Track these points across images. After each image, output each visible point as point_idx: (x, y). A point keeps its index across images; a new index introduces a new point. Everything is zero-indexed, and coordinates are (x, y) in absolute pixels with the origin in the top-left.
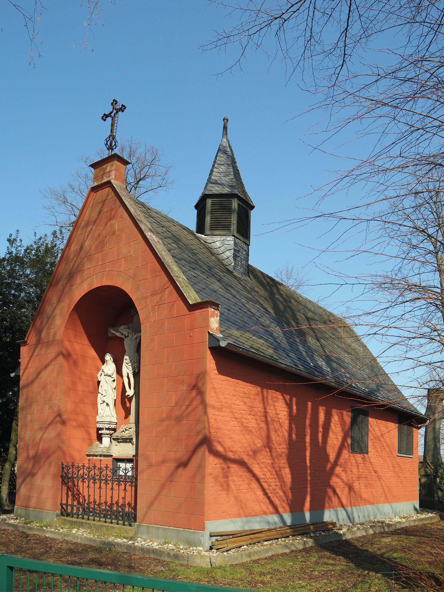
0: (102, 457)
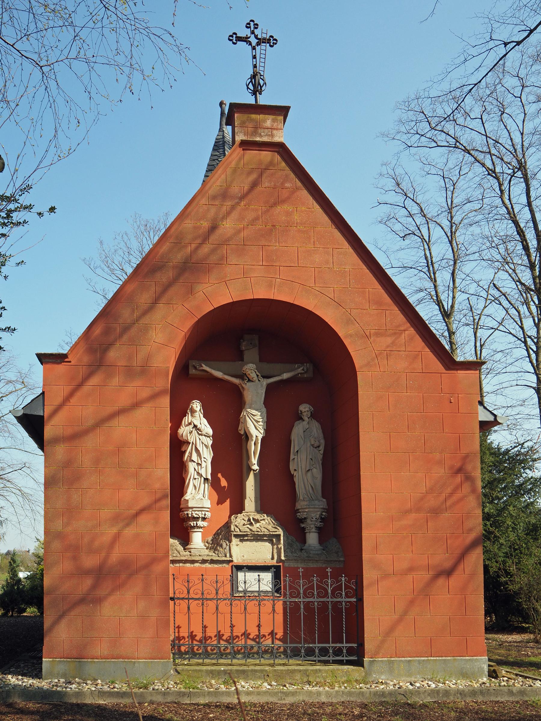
0: (207, 564)
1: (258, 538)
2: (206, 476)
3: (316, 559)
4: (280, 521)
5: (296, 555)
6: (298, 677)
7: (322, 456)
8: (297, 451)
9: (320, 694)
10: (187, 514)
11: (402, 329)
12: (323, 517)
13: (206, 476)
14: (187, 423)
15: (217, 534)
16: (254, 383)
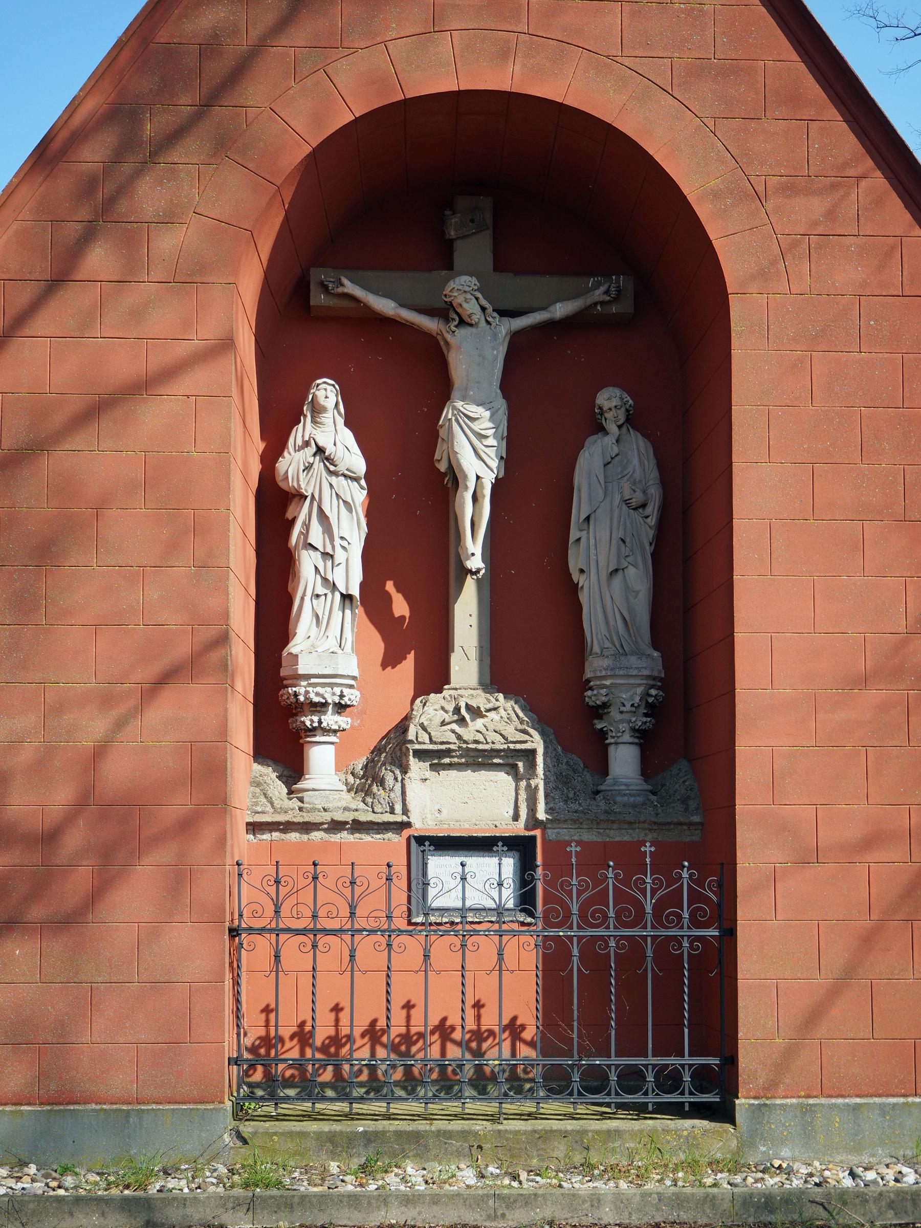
0: (344, 834)
1: (478, 759)
2: (347, 589)
3: (628, 819)
4: (540, 714)
5: (575, 806)
6: (559, 1150)
7: (651, 533)
8: (588, 519)
9: (599, 1200)
10: (296, 695)
11: (851, 172)
12: (651, 700)
13: (347, 589)
14: (299, 442)
15: (378, 750)
16: (473, 330)
